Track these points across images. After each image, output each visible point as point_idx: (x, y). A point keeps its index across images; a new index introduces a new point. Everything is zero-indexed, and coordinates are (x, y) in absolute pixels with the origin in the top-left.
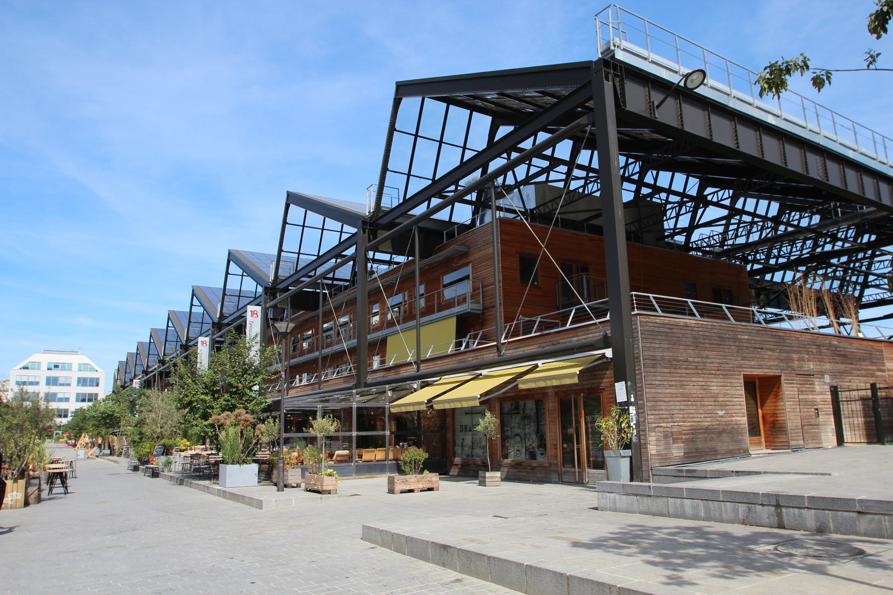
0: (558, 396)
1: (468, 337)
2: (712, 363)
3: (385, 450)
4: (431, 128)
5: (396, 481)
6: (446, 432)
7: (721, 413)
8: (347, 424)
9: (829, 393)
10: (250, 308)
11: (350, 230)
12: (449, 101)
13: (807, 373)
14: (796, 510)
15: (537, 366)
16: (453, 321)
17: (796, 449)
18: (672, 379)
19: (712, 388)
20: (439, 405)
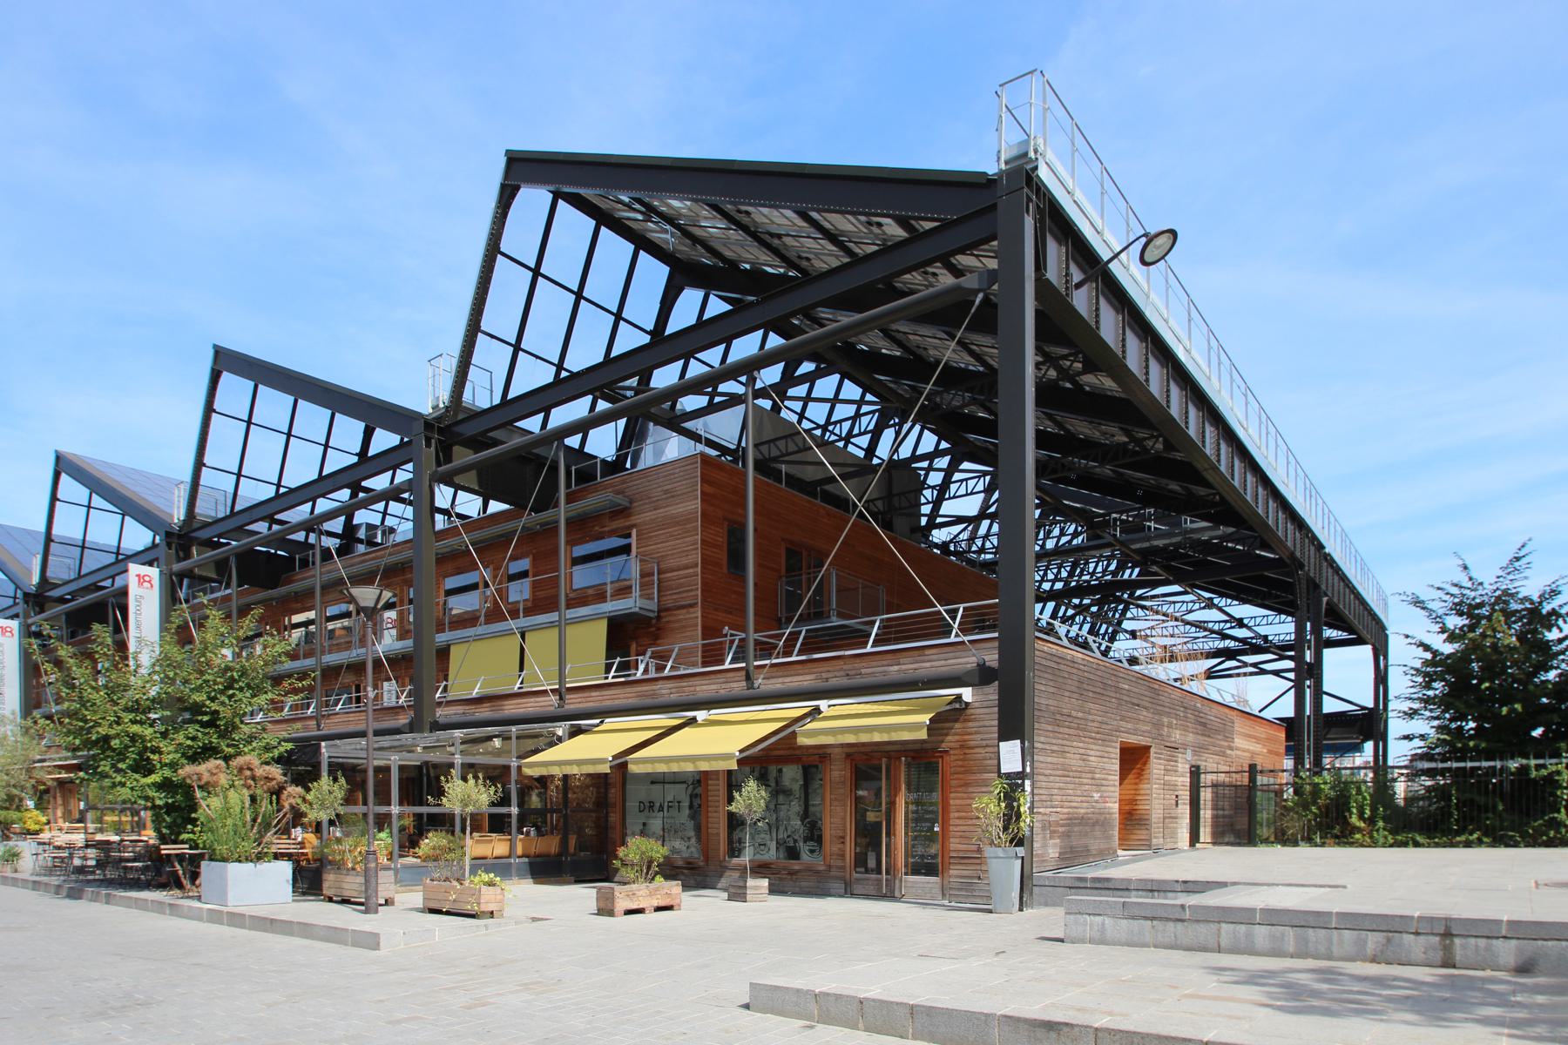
0: (852, 760)
1: (649, 654)
2: (1093, 721)
3: (510, 840)
4: (564, 262)
5: (617, 893)
6: (607, 813)
7: (1096, 796)
9: (1188, 775)
12: (604, 219)
13: (1173, 745)
14: (1482, 942)
15: (817, 710)
16: (603, 626)
17: (1157, 851)
18: (1054, 741)
19: (1091, 758)
20: (641, 766)
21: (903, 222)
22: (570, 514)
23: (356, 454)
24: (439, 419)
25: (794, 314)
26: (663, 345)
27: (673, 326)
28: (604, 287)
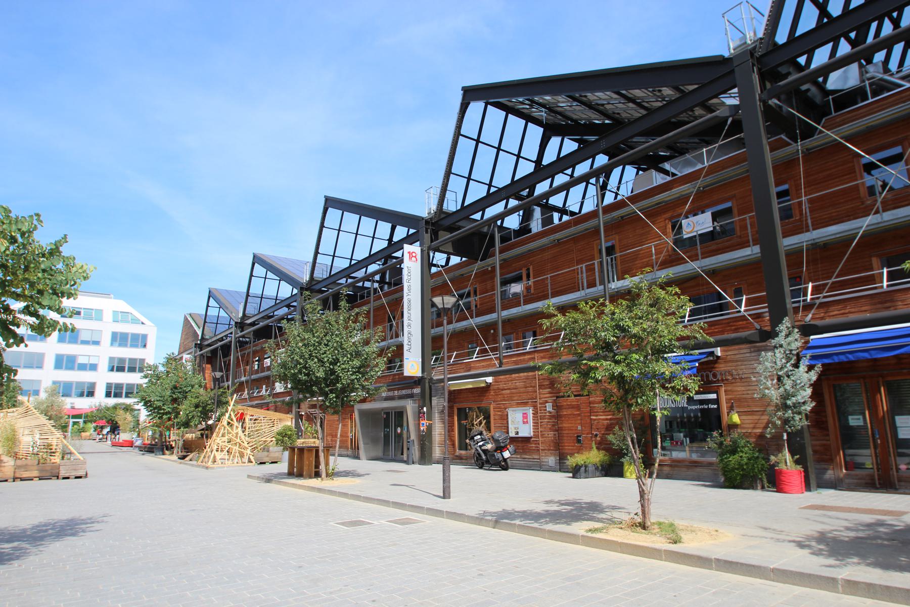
4: (491, 135)
12: (509, 110)
21: (676, 89)
24: (431, 219)
25: (781, 65)
26: (542, 171)
27: (545, 162)
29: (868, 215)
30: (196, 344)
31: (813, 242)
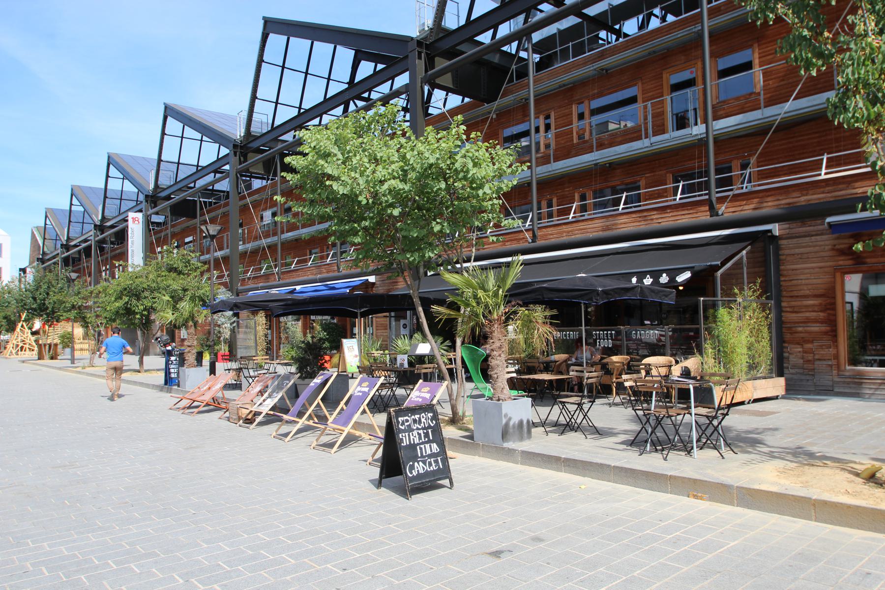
8: (759, 281)
10: (131, 215)
11: (224, 151)
22: (710, 24)
23: (347, 83)
24: (425, 38)
28: (320, 66)
29: (788, 101)
30: (38, 259)
31: (595, 162)
